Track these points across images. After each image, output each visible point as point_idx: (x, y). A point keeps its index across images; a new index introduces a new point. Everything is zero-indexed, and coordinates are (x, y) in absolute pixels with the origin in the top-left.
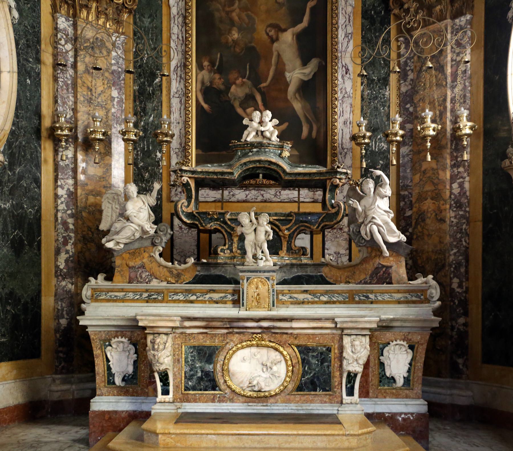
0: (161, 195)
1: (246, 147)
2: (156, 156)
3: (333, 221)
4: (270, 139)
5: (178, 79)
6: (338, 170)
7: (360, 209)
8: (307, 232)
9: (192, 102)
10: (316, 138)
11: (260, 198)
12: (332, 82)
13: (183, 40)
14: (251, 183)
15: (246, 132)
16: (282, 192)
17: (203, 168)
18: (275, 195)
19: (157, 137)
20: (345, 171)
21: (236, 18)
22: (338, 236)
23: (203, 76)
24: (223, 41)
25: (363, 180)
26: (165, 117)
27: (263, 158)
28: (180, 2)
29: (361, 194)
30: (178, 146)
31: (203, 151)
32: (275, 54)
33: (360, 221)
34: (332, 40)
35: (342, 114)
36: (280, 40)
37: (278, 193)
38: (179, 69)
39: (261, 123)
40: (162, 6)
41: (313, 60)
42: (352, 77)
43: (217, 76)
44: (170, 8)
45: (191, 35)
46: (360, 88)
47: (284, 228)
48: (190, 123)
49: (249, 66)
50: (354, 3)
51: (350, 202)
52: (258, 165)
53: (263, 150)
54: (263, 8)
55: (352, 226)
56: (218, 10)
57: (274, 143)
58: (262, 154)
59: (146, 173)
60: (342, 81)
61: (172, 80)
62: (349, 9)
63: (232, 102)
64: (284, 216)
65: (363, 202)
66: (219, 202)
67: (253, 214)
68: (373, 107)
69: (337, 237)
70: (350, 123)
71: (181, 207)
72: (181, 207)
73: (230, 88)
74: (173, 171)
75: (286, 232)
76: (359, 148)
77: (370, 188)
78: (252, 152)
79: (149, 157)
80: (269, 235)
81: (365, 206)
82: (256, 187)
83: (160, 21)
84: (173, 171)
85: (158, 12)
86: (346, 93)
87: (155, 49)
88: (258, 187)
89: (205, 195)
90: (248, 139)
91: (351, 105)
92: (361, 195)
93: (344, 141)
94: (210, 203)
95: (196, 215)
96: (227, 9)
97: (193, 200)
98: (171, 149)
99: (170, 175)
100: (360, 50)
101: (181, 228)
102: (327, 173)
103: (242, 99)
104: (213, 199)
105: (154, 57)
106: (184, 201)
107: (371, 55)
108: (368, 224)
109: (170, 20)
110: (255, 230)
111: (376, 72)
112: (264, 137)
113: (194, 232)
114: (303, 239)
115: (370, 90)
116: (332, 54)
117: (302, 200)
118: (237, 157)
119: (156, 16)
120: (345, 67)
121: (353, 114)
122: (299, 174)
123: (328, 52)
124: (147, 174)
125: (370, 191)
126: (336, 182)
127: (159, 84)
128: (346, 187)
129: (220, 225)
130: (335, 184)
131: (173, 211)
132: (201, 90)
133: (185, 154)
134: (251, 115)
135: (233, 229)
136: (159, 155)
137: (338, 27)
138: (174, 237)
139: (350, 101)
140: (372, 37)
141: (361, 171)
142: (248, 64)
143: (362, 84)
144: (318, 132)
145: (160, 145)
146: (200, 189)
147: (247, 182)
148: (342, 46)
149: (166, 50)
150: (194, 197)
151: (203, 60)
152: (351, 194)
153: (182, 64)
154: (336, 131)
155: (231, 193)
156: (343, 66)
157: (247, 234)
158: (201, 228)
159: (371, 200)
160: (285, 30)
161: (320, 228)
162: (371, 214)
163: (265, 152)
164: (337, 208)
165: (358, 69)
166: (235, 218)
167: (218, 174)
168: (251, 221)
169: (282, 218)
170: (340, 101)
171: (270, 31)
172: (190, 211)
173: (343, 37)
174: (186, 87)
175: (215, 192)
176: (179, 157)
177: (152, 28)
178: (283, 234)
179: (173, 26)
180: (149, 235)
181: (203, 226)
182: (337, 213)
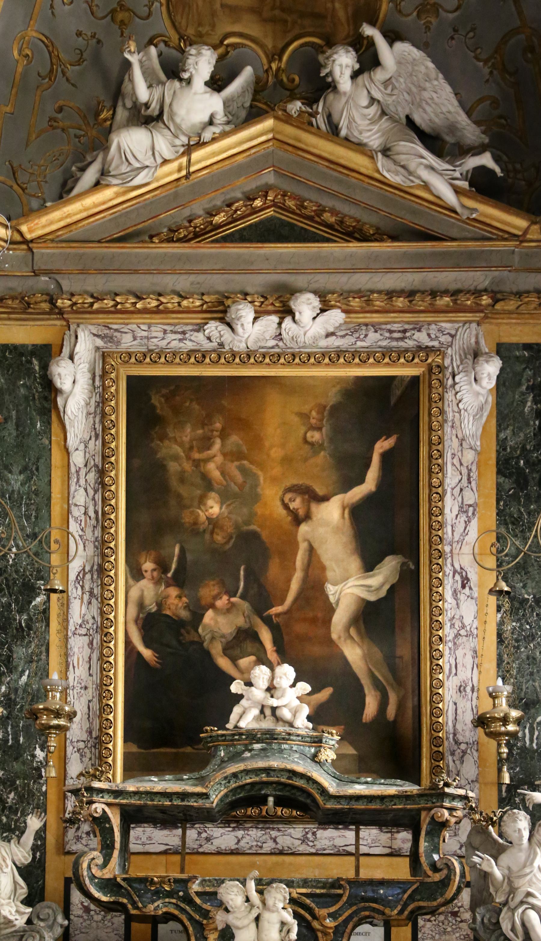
0: (44, 839)
1: (238, 740)
2: (34, 756)
3: (435, 900)
4: (291, 725)
5: (86, 597)
6: (447, 790)
7: (498, 874)
8: (375, 921)
9: (115, 645)
10: (395, 721)
11: (269, 846)
12: (431, 604)
13: (97, 519)
14: (249, 813)
15: (237, 710)
16: (320, 833)
17: (139, 785)
18: (304, 840)
19: (37, 718)
20: (461, 792)
21: (216, 474)
22: (449, 929)
23: (142, 591)
24: (187, 518)
25: (505, 813)
26: (55, 676)
27: (275, 763)
28: (92, 442)
29: (501, 841)
30: (85, 737)
31: (139, 747)
32: (303, 547)
33: (500, 899)
34: (430, 519)
35: (454, 671)
36: (314, 519)
37: (310, 836)
38: (88, 576)
39: (271, 689)
40: (50, 450)
41: (388, 559)
42: (476, 595)
43: (173, 592)
44: (68, 453)
45: (115, 509)
46: (494, 618)
47: (324, 912)
48: (111, 674)
49: (246, 571)
50: (478, 443)
51: (476, 859)
52: (264, 777)
53: (275, 746)
54: (276, 453)
55: (480, 910)
56: (176, 458)
57: (300, 732)
58: (274, 754)
59: (10, 793)
60: (454, 602)
61: (72, 600)
62: (469, 456)
63: (205, 644)
64: (323, 888)
65: (504, 859)
66: (176, 853)
67: (252, 885)
68: (524, 656)
69: (445, 932)
70: (473, 690)
71: (89, 868)
72: (89, 868)
73: (203, 615)
74: (71, 791)
75: (329, 922)
76: (493, 743)
77: (520, 830)
78: (250, 751)
79: (16, 759)
80: (289, 931)
81: (509, 868)
82: (259, 822)
83: (46, 480)
84: (71, 791)
85: (42, 461)
86: (463, 627)
87: (34, 536)
88: (265, 822)
89: (144, 839)
90: (243, 724)
91: (475, 652)
92: (500, 844)
93: (459, 727)
94: (154, 857)
95: (123, 883)
96: (196, 456)
97: (116, 853)
98: (68, 742)
99: (65, 797)
100: (494, 540)
101: (87, 910)
102: (420, 795)
103: (230, 638)
104: (163, 848)
105: (31, 554)
106: (98, 856)
107: (519, 551)
108: (516, 908)
109: (69, 478)
110: (257, 919)
111: (530, 584)
112: (278, 719)
113: (119, 919)
114: (367, 934)
115: (519, 620)
116: (431, 547)
117: (363, 849)
118: (216, 761)
119: (37, 469)
120: (460, 574)
121: (480, 672)
122: (358, 798)
123: (421, 543)
124: (12, 795)
125: (521, 837)
126: (442, 815)
127: (42, 608)
128: (466, 826)
129: (177, 906)
130: (440, 820)
131: (70, 874)
132: (136, 621)
133: (100, 752)
134: (249, 673)
135: (206, 914)
136: (40, 754)
137: (445, 491)
138: (71, 930)
139: (472, 643)
140: (521, 513)
141: (500, 791)
142: (242, 568)
143: (499, 608)
144: (401, 706)
145: (43, 735)
146: (132, 826)
147: (240, 812)
148: (453, 531)
149: (58, 537)
150: (117, 845)
151: (142, 560)
152: (477, 840)
153: (95, 567)
154: (440, 705)
155: (204, 835)
156: (455, 572)
157: (238, 928)
158: (133, 912)
159: (522, 856)
160: (325, 499)
161: (406, 913)
162: (523, 886)
163: (281, 751)
164: (445, 872)
165: (491, 579)
166: (212, 890)
167: (174, 797)
168: (248, 900)
169: (318, 891)
170: (450, 644)
171: (292, 500)
172: (108, 876)
173: (455, 512)
174: (102, 613)
175: (166, 832)
176: (86, 759)
177: (28, 494)
178: (322, 925)
179: (76, 491)
180: (13, 929)
181: (137, 908)
182: (445, 883)
